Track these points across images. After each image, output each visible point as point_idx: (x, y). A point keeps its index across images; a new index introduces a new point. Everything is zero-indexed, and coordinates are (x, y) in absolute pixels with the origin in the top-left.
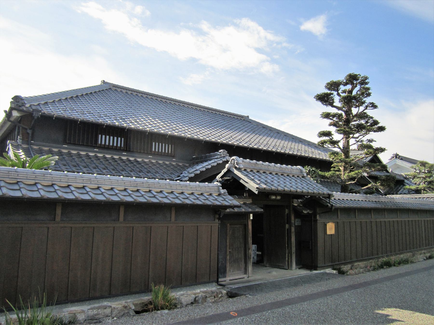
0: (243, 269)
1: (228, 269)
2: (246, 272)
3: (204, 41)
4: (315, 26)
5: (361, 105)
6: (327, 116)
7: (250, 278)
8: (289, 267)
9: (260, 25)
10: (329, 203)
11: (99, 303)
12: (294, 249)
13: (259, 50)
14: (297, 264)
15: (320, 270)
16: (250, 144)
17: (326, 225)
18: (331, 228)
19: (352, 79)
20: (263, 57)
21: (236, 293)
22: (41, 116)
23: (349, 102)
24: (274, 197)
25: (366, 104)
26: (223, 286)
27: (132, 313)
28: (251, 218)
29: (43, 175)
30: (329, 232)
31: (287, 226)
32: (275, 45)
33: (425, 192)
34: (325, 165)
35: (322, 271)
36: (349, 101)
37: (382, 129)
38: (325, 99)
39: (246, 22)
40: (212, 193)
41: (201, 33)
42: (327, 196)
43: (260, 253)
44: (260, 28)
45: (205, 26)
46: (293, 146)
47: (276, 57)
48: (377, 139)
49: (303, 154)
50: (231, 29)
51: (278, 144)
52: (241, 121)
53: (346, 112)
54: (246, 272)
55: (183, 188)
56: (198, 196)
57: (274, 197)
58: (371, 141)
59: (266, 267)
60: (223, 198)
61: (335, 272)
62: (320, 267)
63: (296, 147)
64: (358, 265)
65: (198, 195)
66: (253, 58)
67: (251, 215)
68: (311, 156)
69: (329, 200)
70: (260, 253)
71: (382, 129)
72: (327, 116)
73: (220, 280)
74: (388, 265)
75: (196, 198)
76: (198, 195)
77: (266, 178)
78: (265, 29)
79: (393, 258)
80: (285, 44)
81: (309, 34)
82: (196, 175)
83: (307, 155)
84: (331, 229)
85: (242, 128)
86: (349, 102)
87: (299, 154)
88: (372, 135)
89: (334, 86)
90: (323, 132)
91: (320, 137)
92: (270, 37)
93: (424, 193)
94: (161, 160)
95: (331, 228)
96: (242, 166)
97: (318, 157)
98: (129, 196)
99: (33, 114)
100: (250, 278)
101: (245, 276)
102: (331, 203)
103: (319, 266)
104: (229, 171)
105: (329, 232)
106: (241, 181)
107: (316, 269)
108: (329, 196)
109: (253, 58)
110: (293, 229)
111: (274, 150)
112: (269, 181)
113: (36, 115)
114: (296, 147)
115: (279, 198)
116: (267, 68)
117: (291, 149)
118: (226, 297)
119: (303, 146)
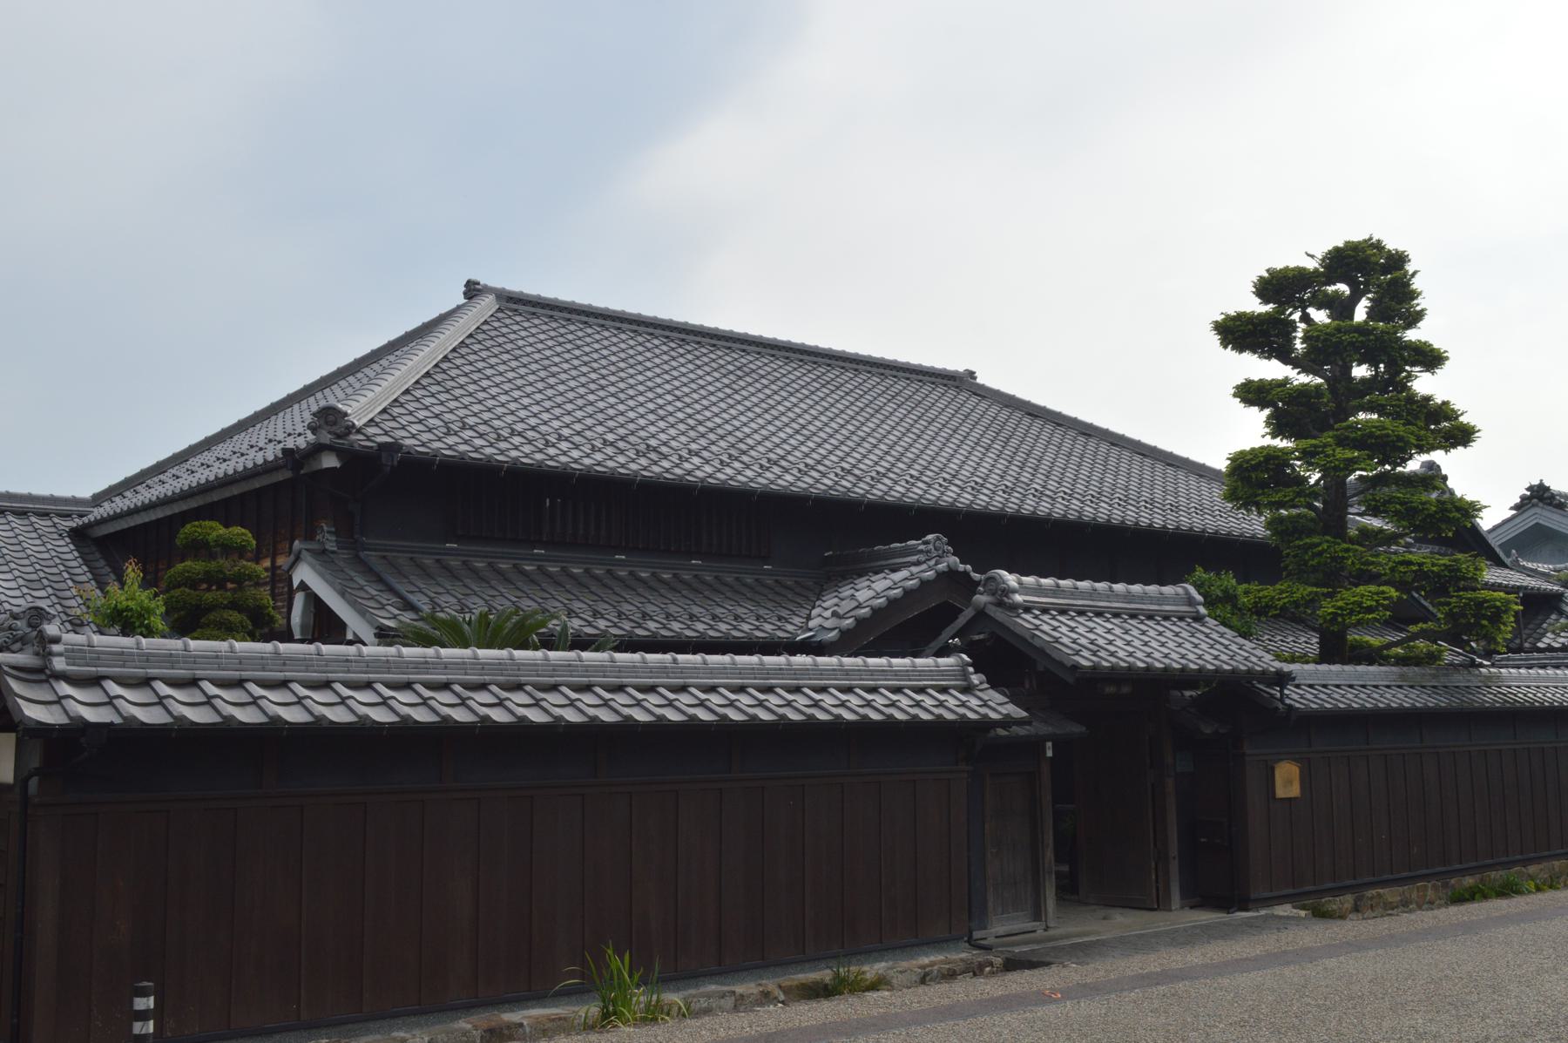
1: (990, 904)
2: (1037, 914)
6: (1252, 393)
7: (1051, 932)
10: (1281, 700)
11: (697, 986)
12: (1174, 850)
14: (1184, 896)
17: (1273, 769)
18: (1288, 780)
24: (1110, 689)
26: (987, 948)
28: (1049, 754)
30: (1281, 793)
38: (1238, 333)
40: (931, 688)
43: (1065, 868)
54: (1037, 914)
57: (1110, 689)
59: (1087, 904)
60: (457, 695)
61: (1303, 913)
62: (1257, 901)
64: (1379, 895)
67: (1049, 744)
69: (1281, 692)
70: (1065, 868)
72: (1252, 393)
73: (977, 934)
77: (1091, 630)
84: (1289, 782)
95: (1288, 780)
100: (1051, 932)
102: (1288, 701)
103: (1253, 896)
105: (1281, 793)
107: (1247, 910)
112: (1101, 642)
115: (1126, 689)
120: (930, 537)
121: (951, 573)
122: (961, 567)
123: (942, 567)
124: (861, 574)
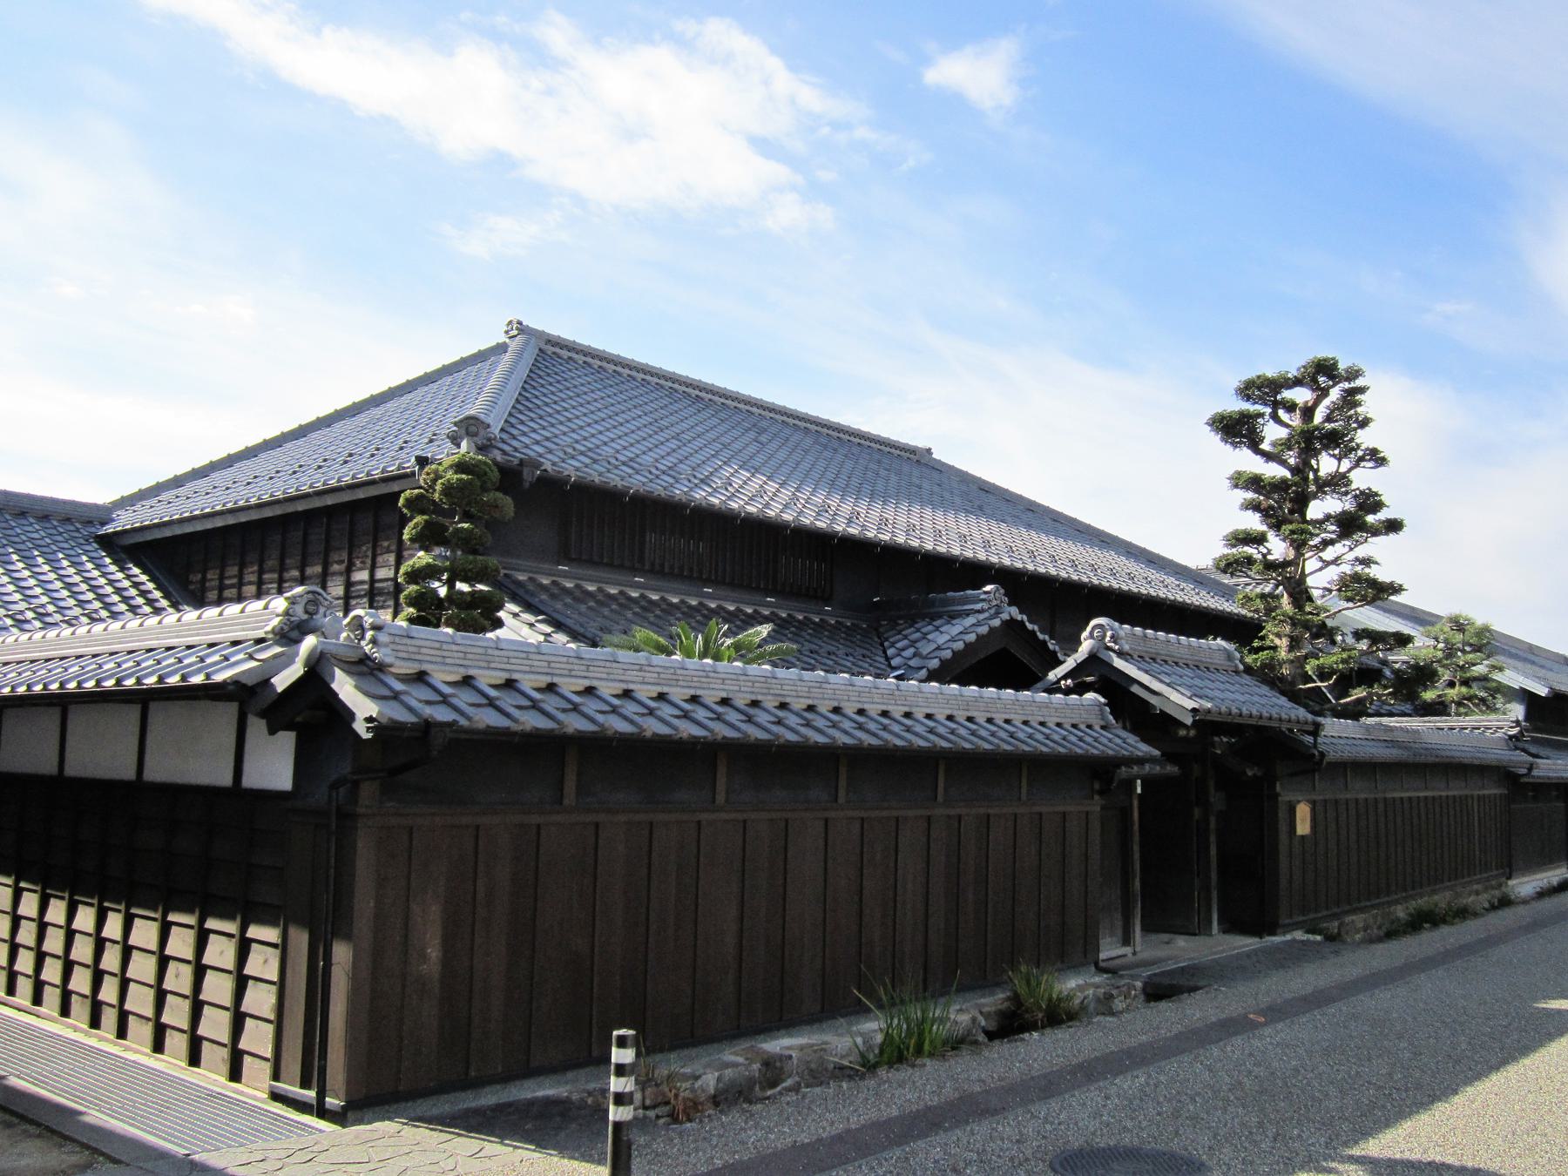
0: (1119, 932)
2: (1127, 940)
3: (550, 92)
4: (979, 75)
5: (1346, 456)
8: (1202, 929)
9: (774, 50)
13: (764, 146)
15: (1284, 934)
16: (729, 498)
19: (1322, 372)
20: (777, 171)
21: (1172, 986)
22: (539, 479)
23: (1301, 440)
25: (1360, 453)
27: (981, 1038)
28: (1139, 790)
29: (437, 645)
31: (1197, 812)
32: (826, 130)
33: (1462, 710)
34: (1242, 631)
35: (1288, 937)
36: (1310, 442)
37: (1394, 526)
38: (1237, 429)
39: (722, 33)
40: (1046, 714)
41: (537, 56)
42: (1311, 728)
44: (775, 64)
45: (557, 34)
46: (915, 521)
47: (826, 176)
48: (1386, 558)
49: (901, 539)
50: (661, 57)
51: (737, 482)
52: (738, 418)
53: (1295, 471)
54: (1127, 940)
55: (633, 675)
56: (577, 699)
58: (1367, 562)
61: (1319, 938)
63: (928, 525)
65: (538, 690)
66: (736, 174)
68: (929, 546)
71: (1394, 526)
74: (1423, 920)
75: (607, 708)
76: (538, 690)
78: (793, 68)
79: (1440, 899)
80: (862, 133)
81: (953, 103)
82: (943, 662)
83: (915, 543)
85: (737, 446)
86: (1301, 440)
87: (885, 537)
88: (1374, 547)
89: (1265, 390)
90: (1245, 532)
91: (1234, 546)
92: (811, 98)
93: (1458, 714)
94: (800, 611)
96: (1127, 647)
97: (956, 551)
98: (533, 707)
99: (521, 473)
100: (1140, 956)
101: (1127, 950)
104: (1093, 658)
106: (1135, 689)
107: (1273, 933)
108: (1316, 730)
109: (736, 174)
110: (1213, 820)
111: (788, 517)
113: (528, 476)
114: (928, 525)
116: (789, 214)
117: (910, 528)
118: (1142, 997)
119: (928, 512)
120: (988, 588)
121: (1011, 624)
122: (1019, 618)
123: (1005, 616)
124: (912, 621)
